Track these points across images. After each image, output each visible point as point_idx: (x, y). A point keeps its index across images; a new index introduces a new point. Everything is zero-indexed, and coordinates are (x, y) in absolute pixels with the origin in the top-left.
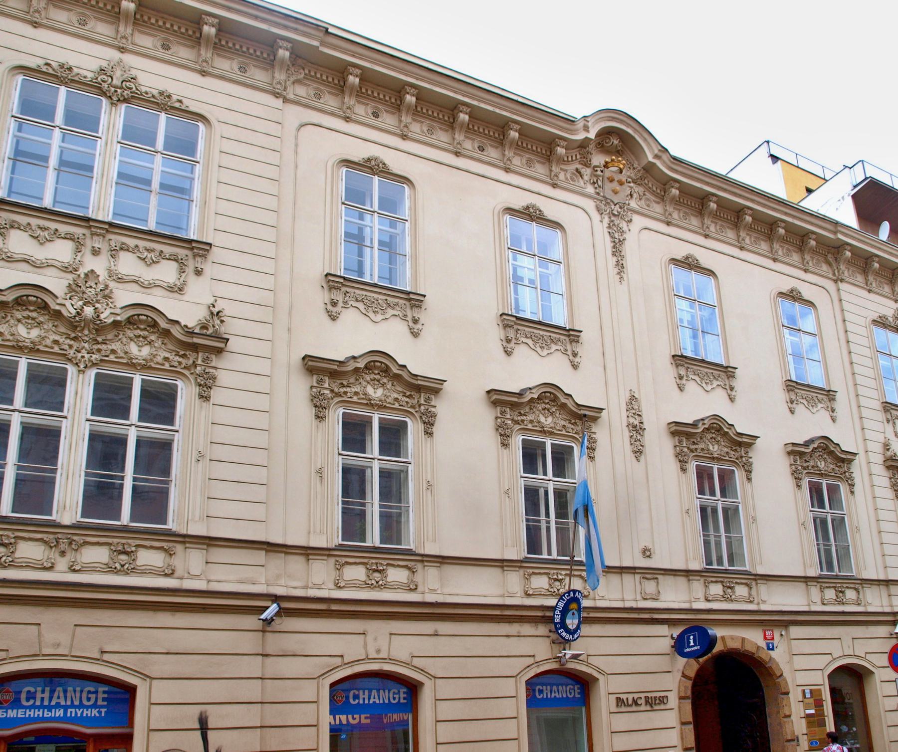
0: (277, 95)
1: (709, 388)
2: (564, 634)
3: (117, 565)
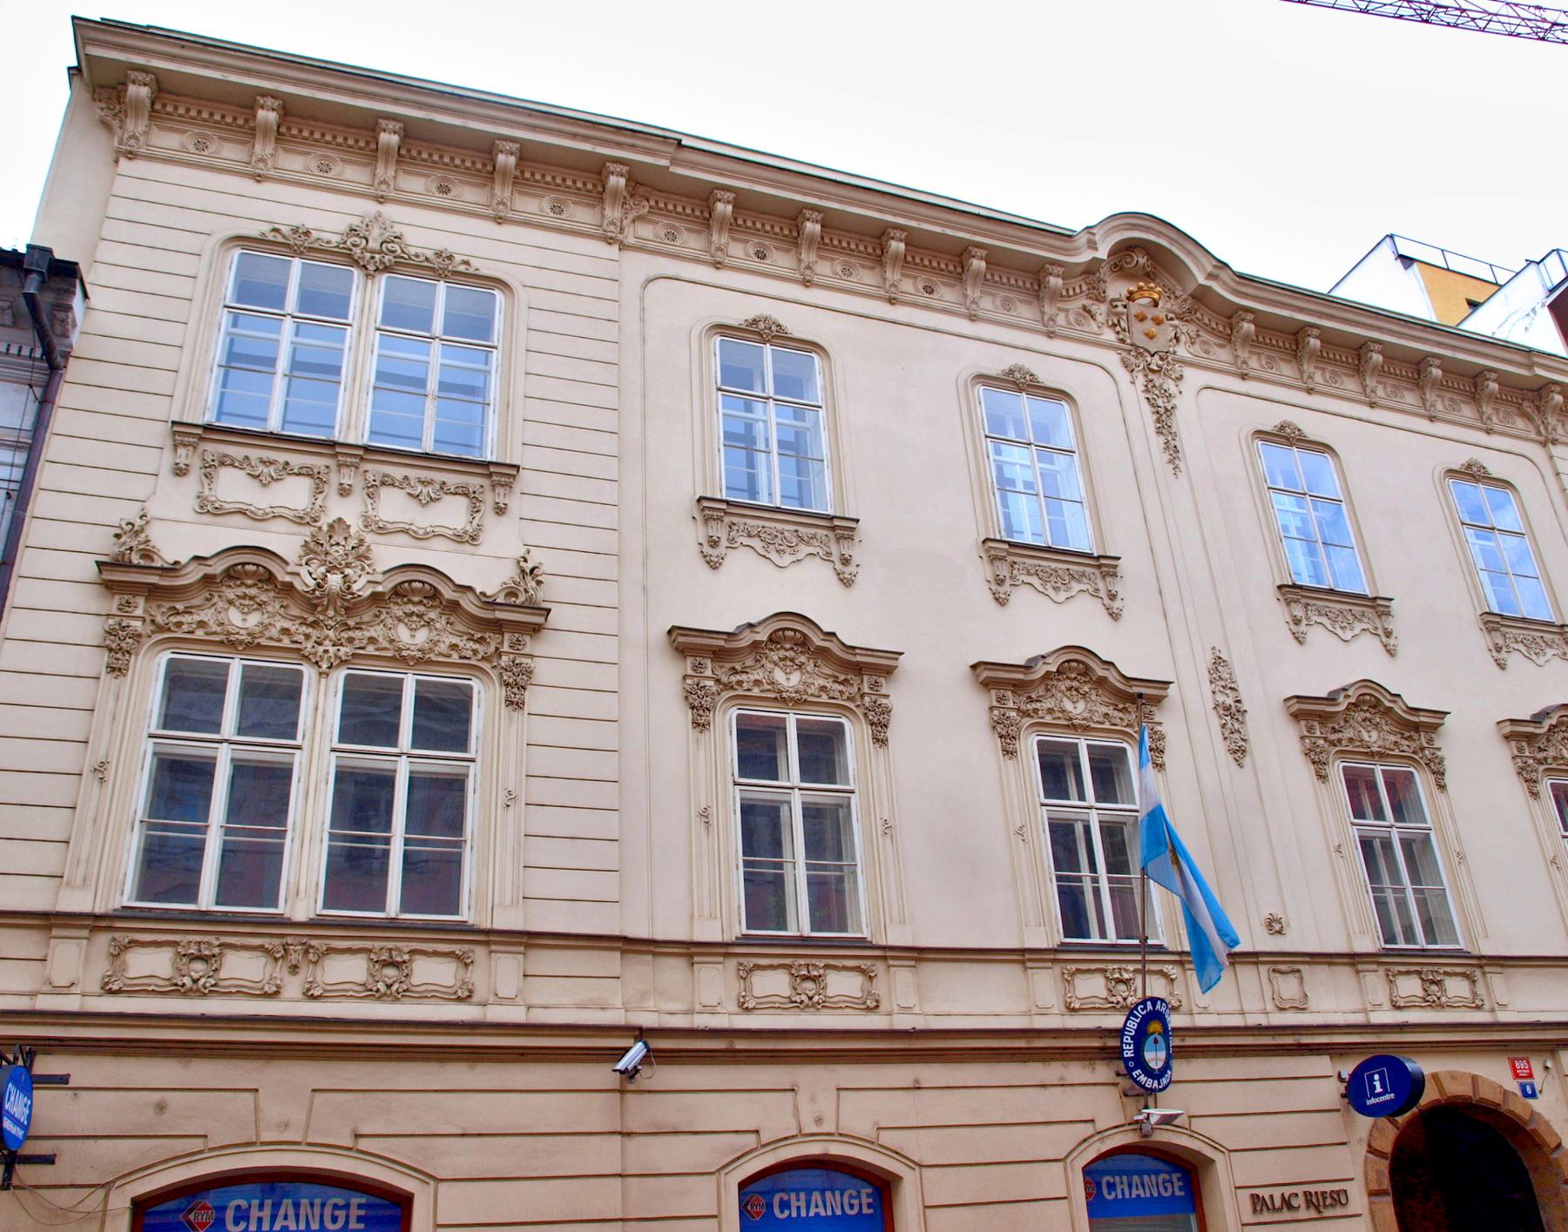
0: (609, 241)
1: (1348, 635)
2: (1143, 1078)
3: (381, 986)
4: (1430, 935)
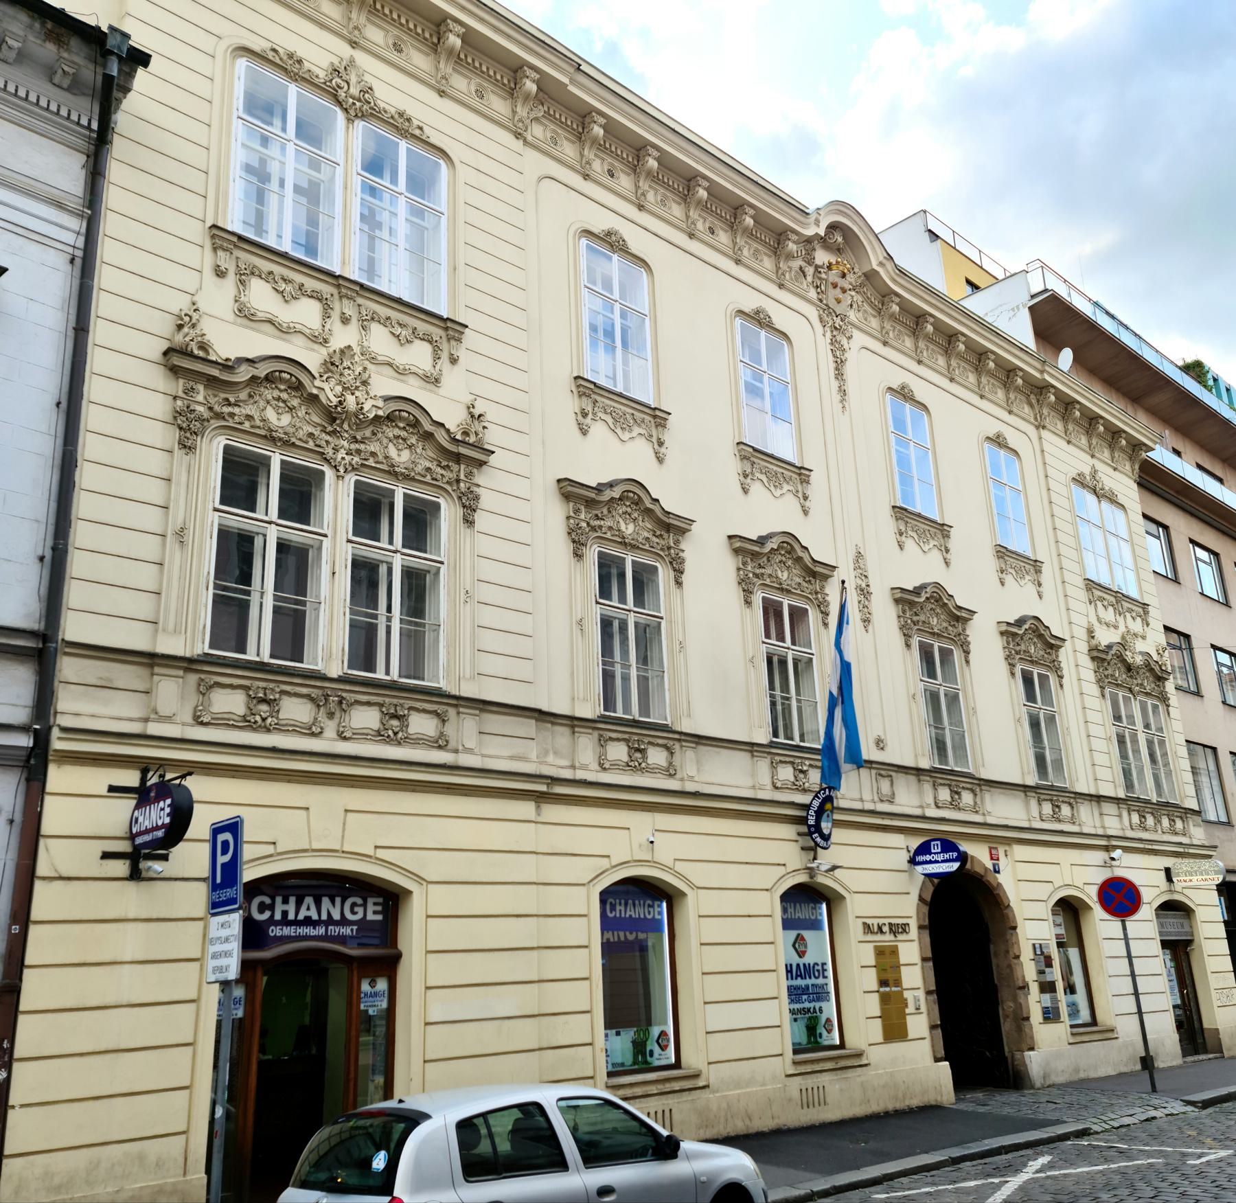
0: (518, 135)
2: (818, 840)
4: (802, 740)
